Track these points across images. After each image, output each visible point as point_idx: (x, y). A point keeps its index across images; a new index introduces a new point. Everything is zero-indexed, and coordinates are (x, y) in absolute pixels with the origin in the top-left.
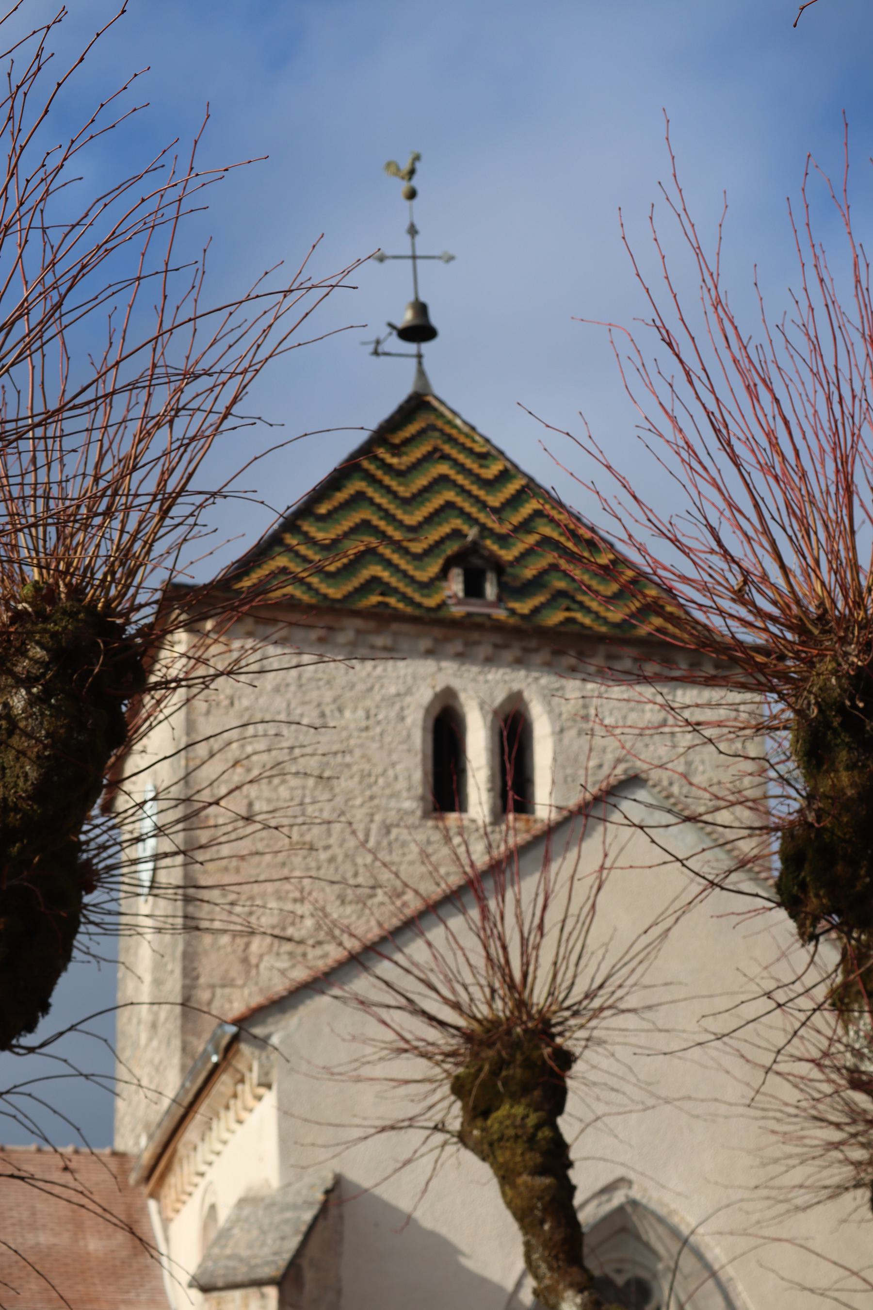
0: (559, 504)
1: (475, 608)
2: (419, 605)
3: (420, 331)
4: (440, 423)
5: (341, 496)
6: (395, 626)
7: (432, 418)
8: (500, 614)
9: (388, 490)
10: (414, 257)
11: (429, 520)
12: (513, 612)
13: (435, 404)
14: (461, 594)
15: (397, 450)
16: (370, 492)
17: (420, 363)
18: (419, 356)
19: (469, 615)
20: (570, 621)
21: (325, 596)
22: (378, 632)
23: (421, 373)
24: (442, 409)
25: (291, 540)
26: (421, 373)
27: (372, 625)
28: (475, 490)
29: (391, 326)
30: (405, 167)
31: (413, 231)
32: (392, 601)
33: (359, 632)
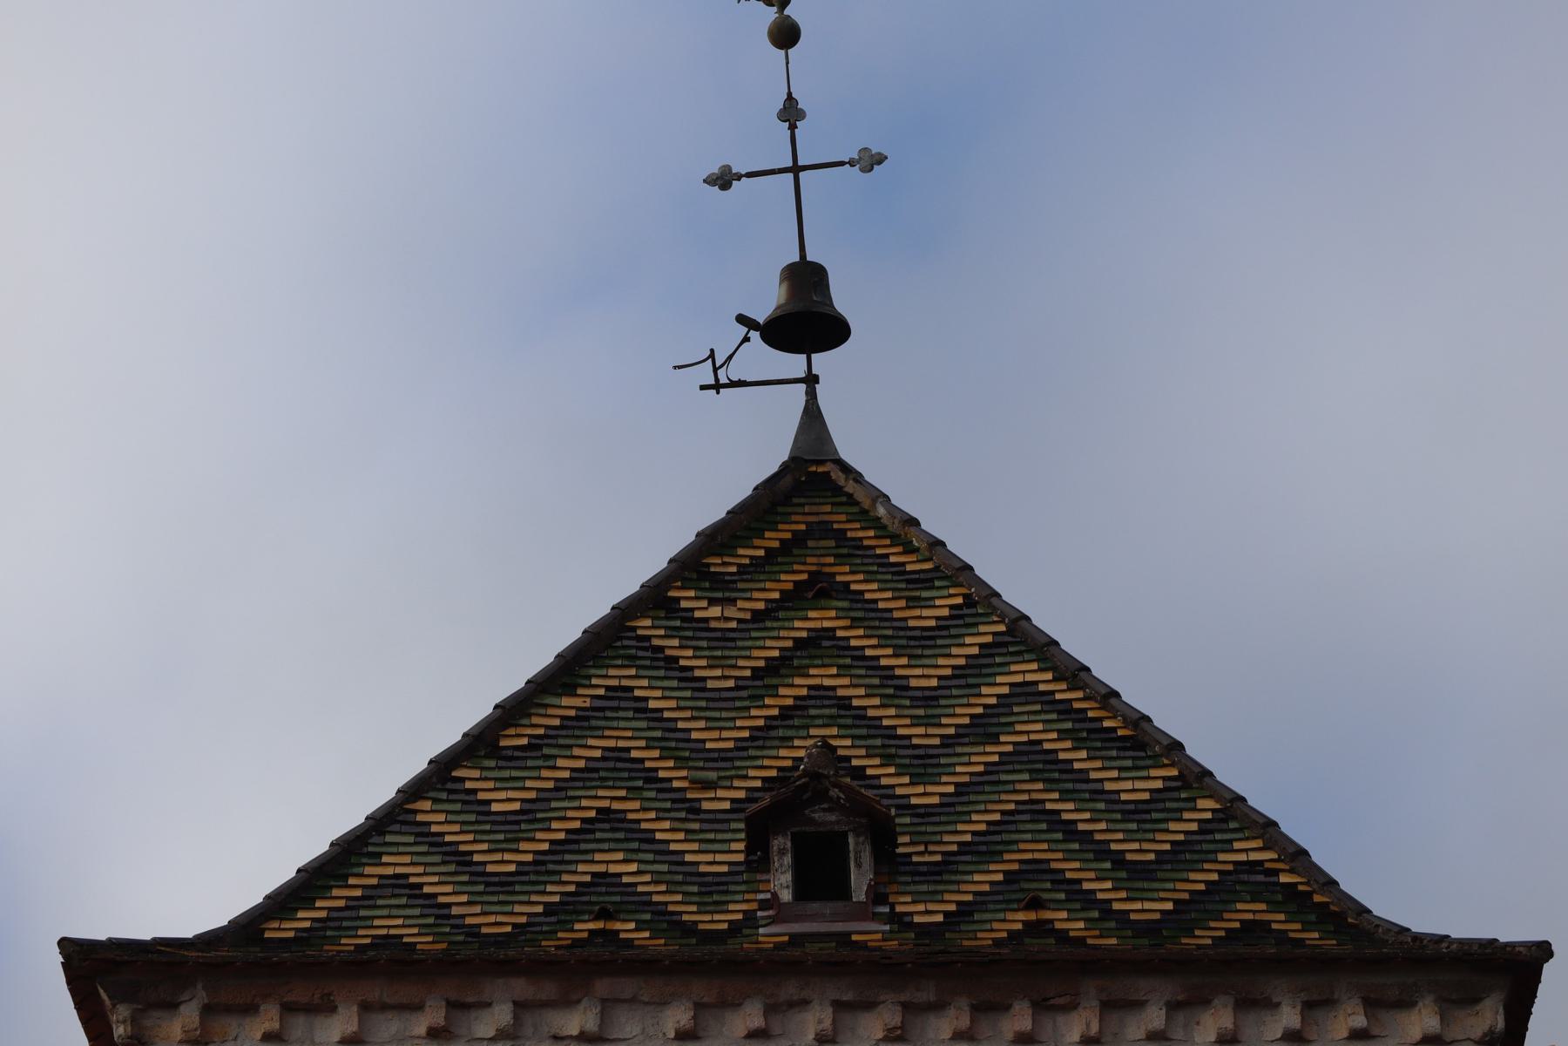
0: (1076, 674)
1: (820, 922)
2: (690, 929)
4: (839, 521)
5: (788, 695)
6: (602, 987)
8: (870, 932)
9: (687, 678)
10: (796, 169)
11: (761, 737)
12: (900, 922)
13: (838, 476)
14: (786, 896)
16: (641, 687)
17: (812, 395)
18: (811, 380)
19: (796, 940)
20: (1038, 929)
21: (473, 931)
22: (566, 1002)
24: (850, 487)
26: (812, 416)
27: (549, 990)
29: (742, 319)
31: (791, 113)
32: (626, 928)
33: (520, 1006)
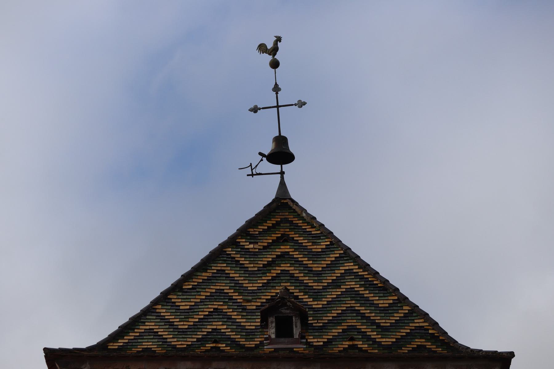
3: (281, 154)
7: (286, 214)
8: (300, 348)
10: (278, 107)
11: (266, 285)
15: (253, 239)
17: (282, 178)
18: (282, 173)
19: (276, 350)
21: (174, 347)
23: (282, 184)
24: (294, 207)
25: (162, 310)
26: (282, 184)
28: (305, 261)
29: (260, 154)
30: (270, 46)
32: (222, 346)
